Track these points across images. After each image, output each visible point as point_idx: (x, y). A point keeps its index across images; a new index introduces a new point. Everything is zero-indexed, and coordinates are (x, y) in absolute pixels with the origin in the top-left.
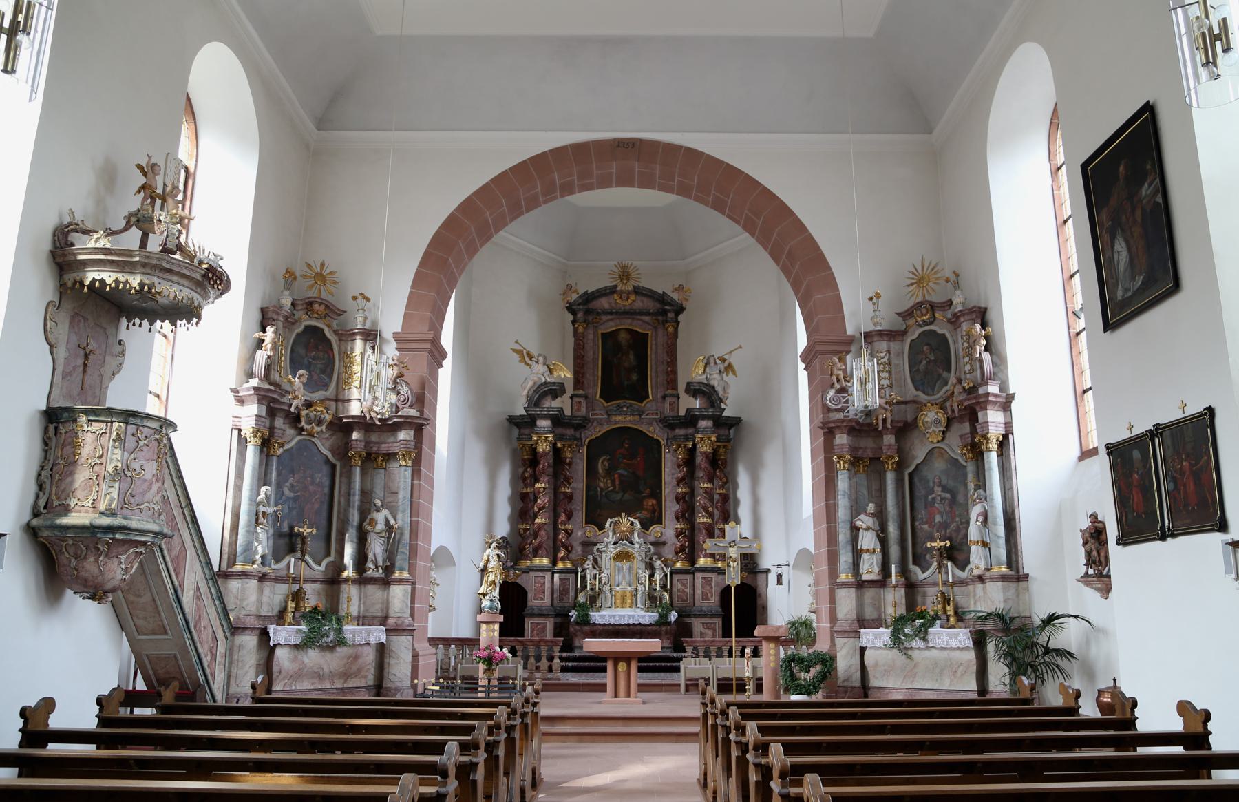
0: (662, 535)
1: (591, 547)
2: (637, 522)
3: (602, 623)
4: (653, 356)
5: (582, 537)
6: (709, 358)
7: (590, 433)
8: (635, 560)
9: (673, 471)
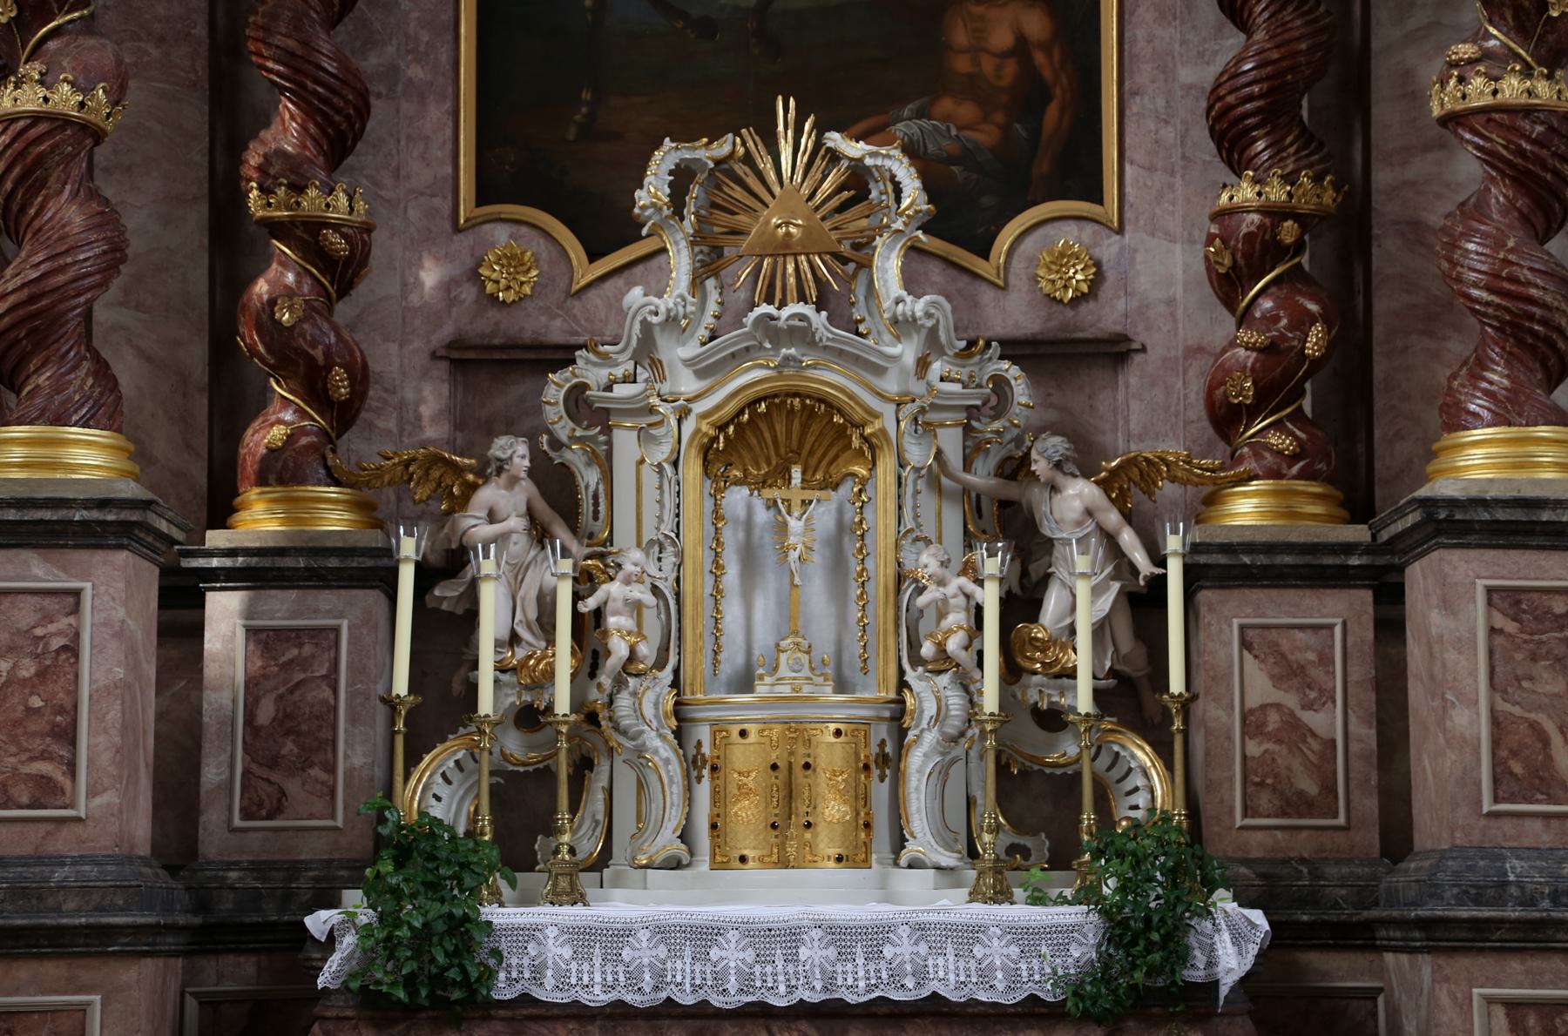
0: (1096, 282)
1: (518, 389)
5: (452, 302)
8: (886, 465)
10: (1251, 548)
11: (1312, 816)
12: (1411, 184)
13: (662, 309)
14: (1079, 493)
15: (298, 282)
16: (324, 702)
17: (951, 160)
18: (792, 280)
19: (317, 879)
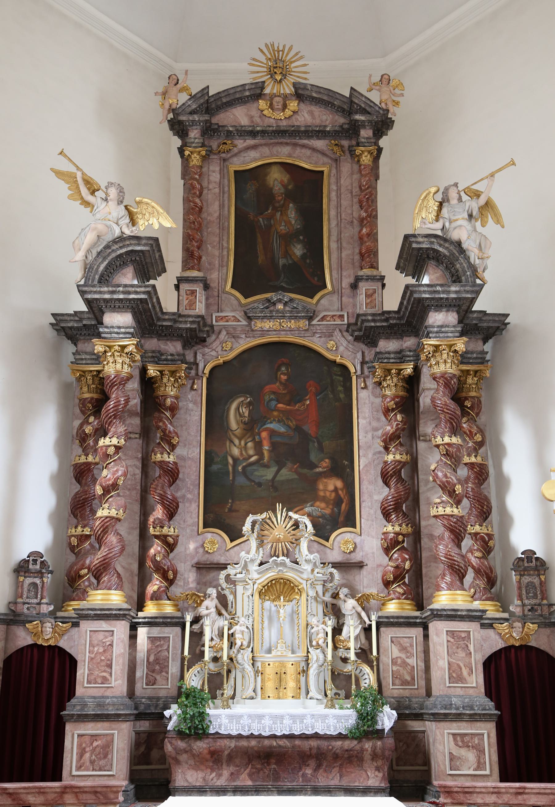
0: (355, 548)
1: (213, 574)
2: (306, 520)
3: (234, 733)
4: (333, 213)
5: (197, 552)
6: (447, 189)
7: (214, 353)
8: (304, 596)
9: (375, 424)
10: (393, 617)
11: (409, 686)
12: (430, 525)
13: (250, 558)
14: (351, 603)
15: (161, 550)
16: (166, 656)
17: (319, 517)
18: (280, 549)
19: (164, 701)
